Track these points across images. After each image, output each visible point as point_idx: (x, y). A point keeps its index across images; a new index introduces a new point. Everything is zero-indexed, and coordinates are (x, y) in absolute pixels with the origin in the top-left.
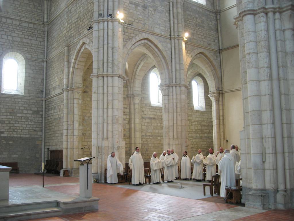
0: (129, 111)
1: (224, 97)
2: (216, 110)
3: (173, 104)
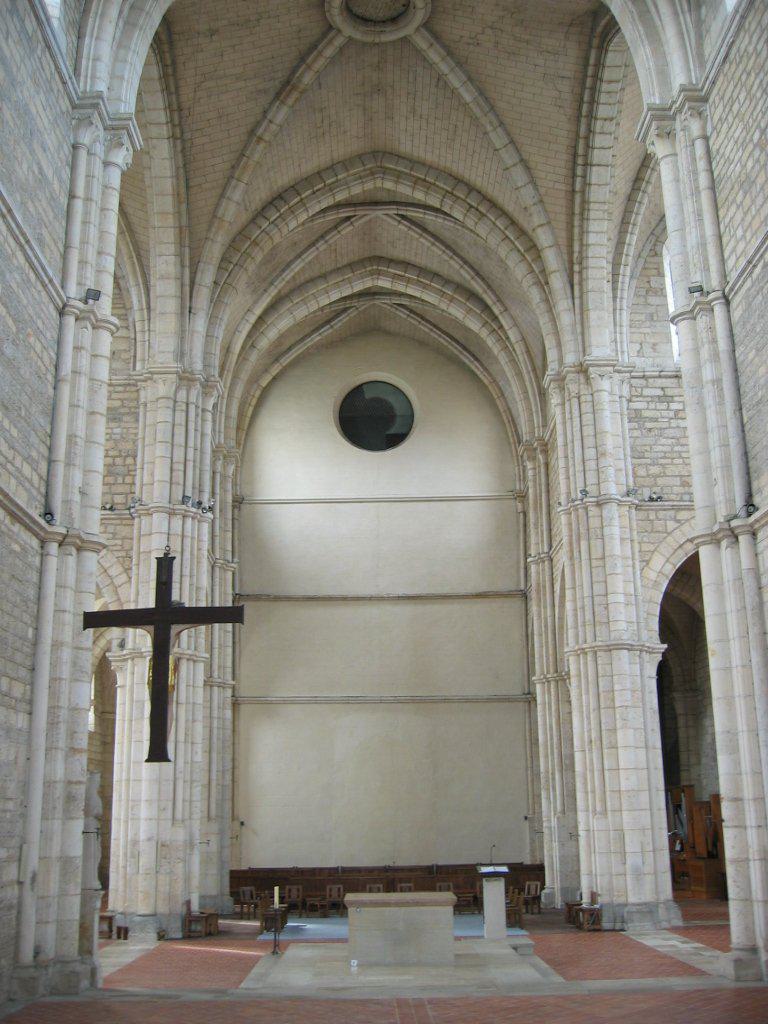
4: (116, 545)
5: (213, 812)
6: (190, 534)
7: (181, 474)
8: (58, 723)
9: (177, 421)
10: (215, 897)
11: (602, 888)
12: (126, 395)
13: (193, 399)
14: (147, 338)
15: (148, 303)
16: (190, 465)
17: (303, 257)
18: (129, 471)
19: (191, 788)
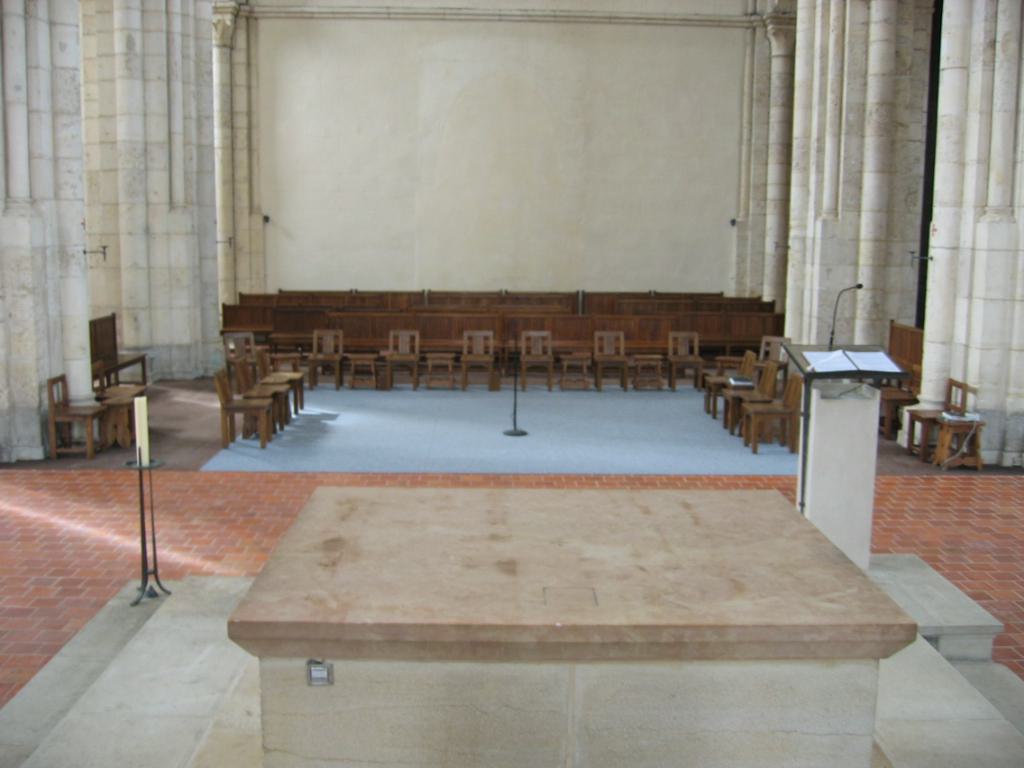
1: (257, 35)
3: (169, 41)
10: (189, 347)
11: (981, 376)
19: (54, 128)
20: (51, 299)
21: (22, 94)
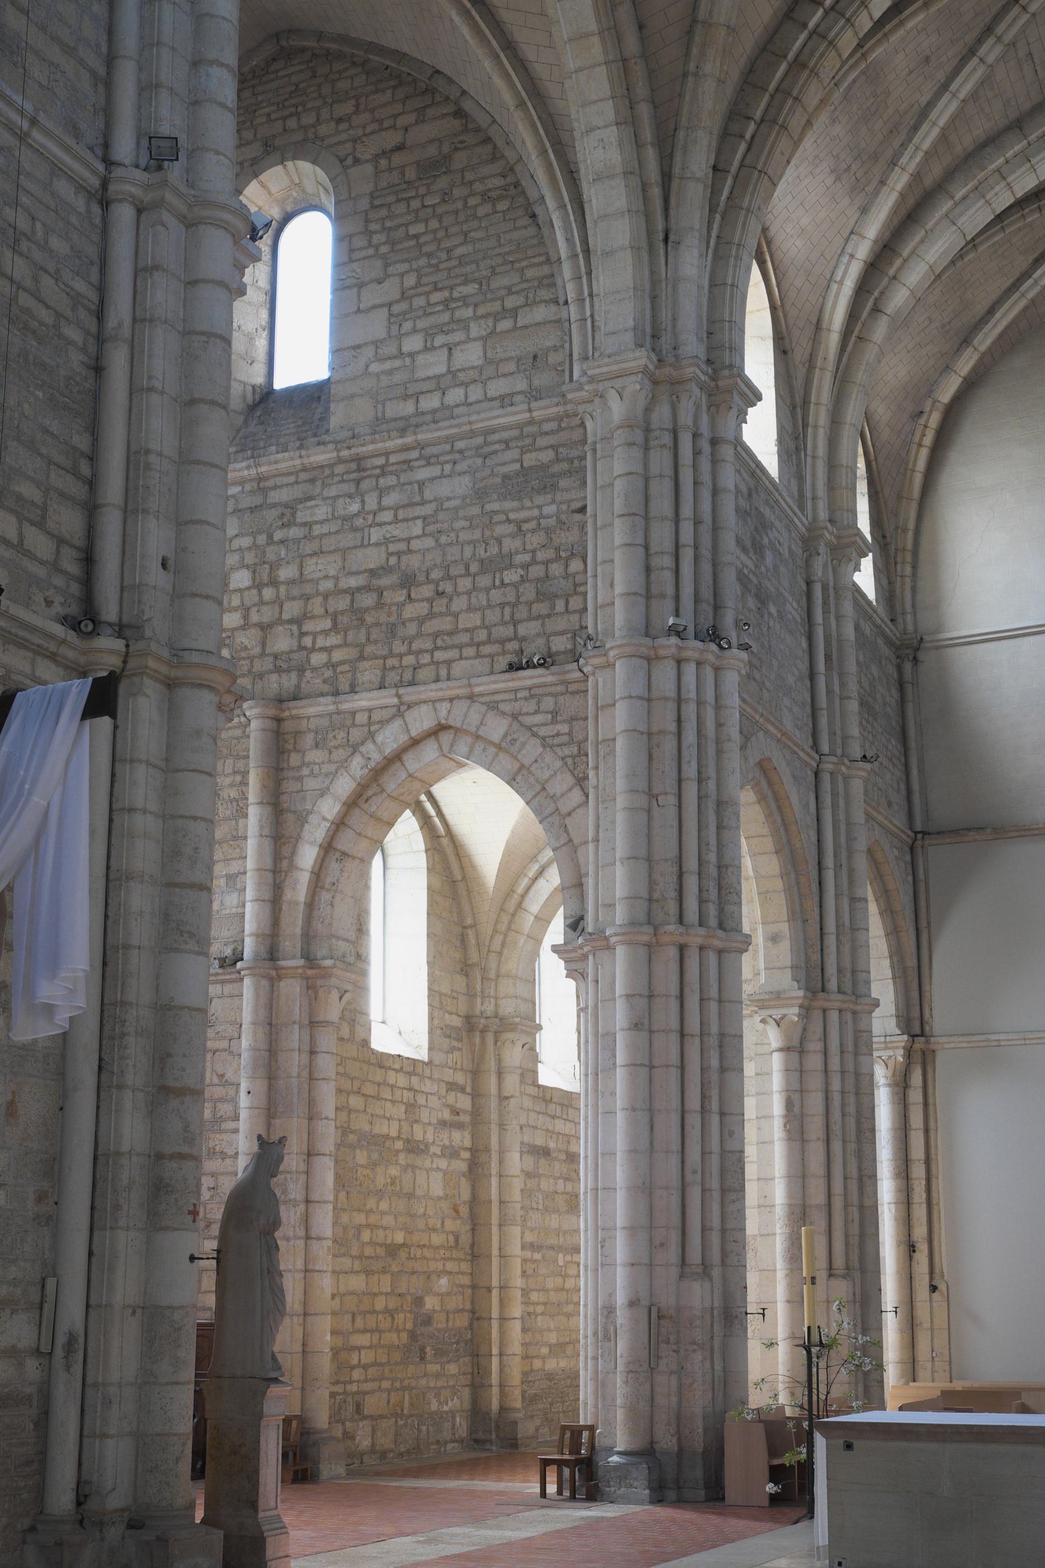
0: (473, 1105)
2: (895, 1129)
4: (558, 735)
5: (839, 1262)
6: (693, 695)
7: (668, 576)
8: (123, 1035)
9: (654, 469)
12: (564, 436)
13: (686, 418)
14: (588, 313)
15: (585, 241)
16: (687, 556)
17: (953, 87)
18: (575, 585)
20: (717, 1355)
21: (698, 1177)
